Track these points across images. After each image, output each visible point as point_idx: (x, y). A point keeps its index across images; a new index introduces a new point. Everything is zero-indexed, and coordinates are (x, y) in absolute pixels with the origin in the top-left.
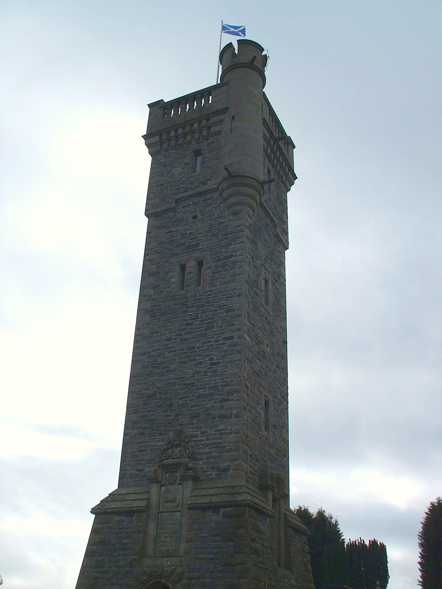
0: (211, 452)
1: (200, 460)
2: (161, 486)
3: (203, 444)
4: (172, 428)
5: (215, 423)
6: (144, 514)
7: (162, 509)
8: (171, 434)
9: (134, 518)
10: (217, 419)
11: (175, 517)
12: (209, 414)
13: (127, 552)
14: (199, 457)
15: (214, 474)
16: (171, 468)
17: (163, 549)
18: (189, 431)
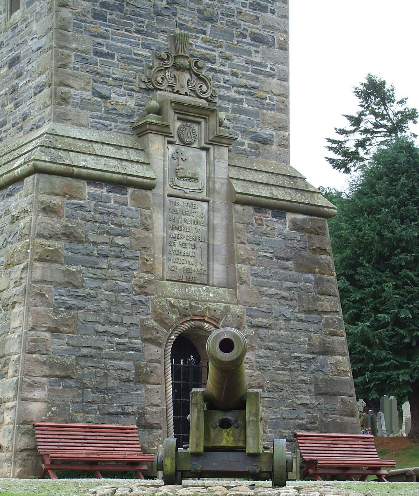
0: (241, 101)
1: (222, 109)
3: (226, 81)
4: (163, 27)
5: (246, 47)
8: (162, 40)
9: (128, 196)
10: (248, 40)
11: (199, 210)
12: (234, 24)
13: (126, 264)
15: (247, 142)
17: (180, 266)
18: (198, 45)
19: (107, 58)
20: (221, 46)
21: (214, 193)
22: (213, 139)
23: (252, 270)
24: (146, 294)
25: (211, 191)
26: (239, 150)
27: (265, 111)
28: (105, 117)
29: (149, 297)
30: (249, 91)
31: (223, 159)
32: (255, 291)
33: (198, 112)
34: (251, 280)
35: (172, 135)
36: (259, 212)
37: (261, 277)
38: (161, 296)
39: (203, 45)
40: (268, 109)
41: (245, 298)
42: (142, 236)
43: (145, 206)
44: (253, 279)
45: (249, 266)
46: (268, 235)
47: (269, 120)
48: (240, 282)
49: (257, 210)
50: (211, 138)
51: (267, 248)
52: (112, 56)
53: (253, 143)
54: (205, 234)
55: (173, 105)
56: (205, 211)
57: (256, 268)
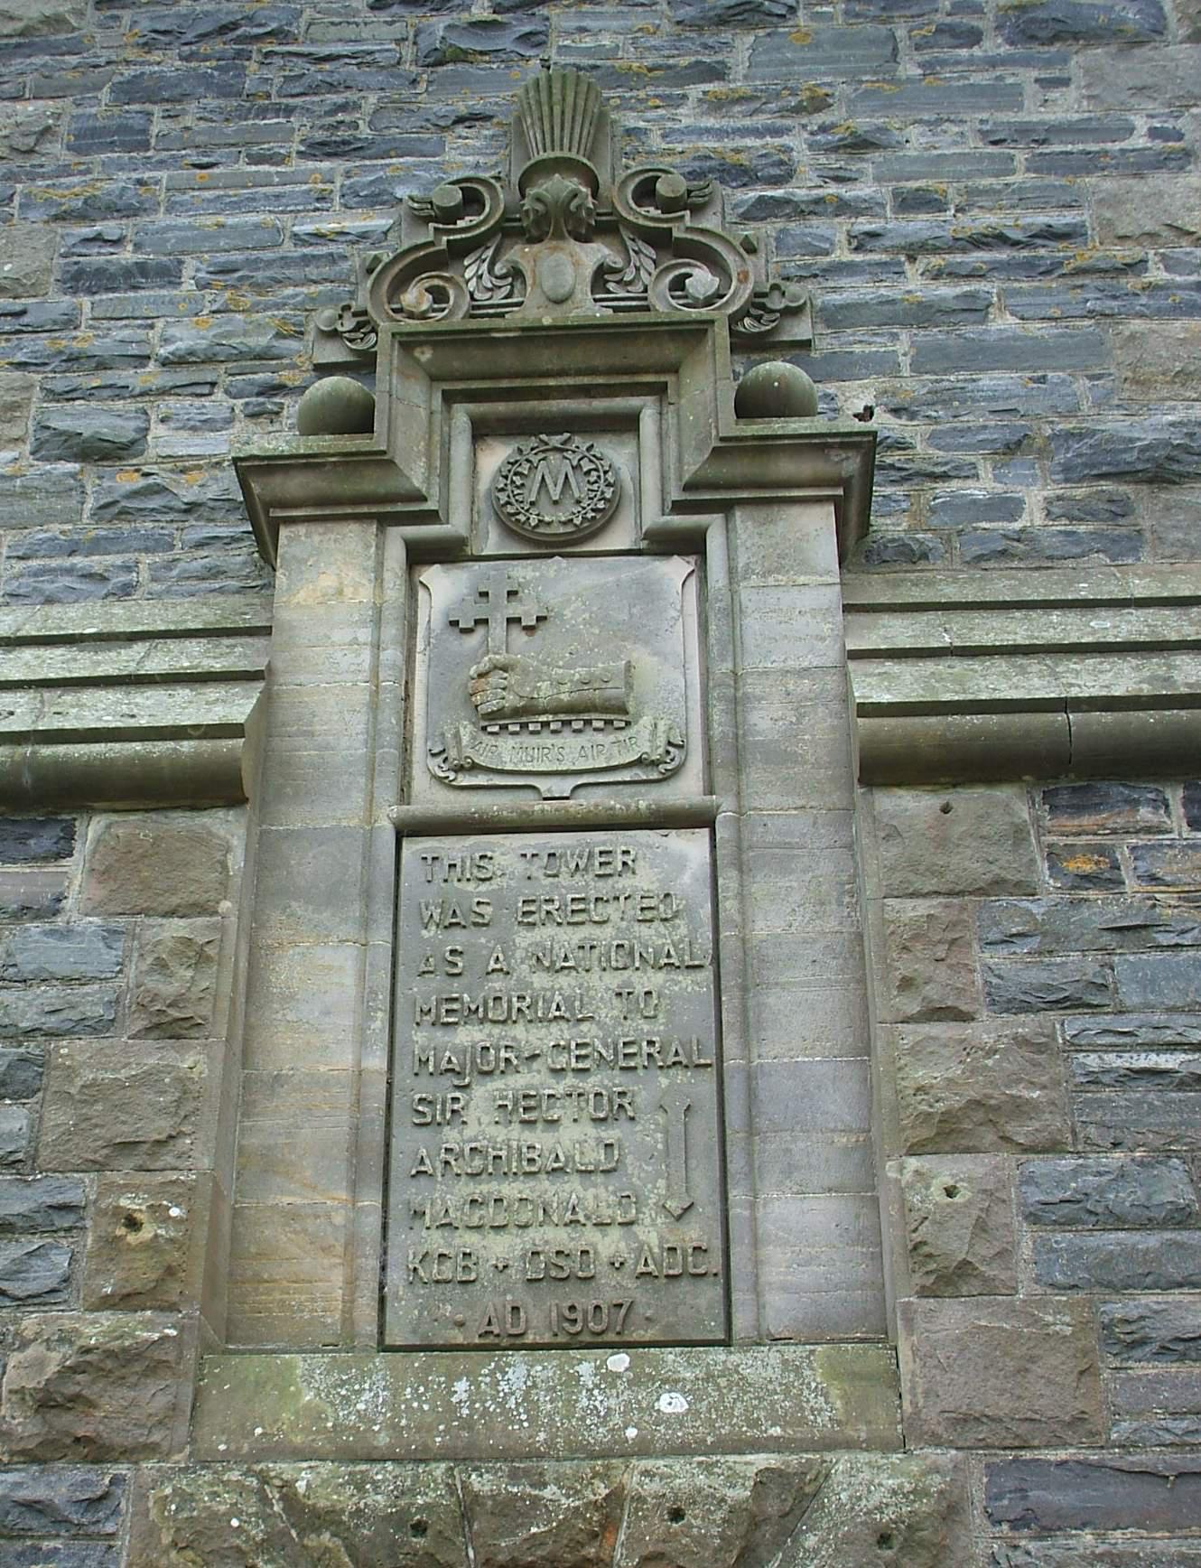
0: (975, 309)
2: (419, 555)
6: (226, 826)
7: (431, 799)
9: (75, 868)
10: (994, 45)
14: (826, 344)
16: (533, 387)
17: (499, 1247)
19: (135, 288)
20: (819, 103)
21: (738, 765)
22: (712, 472)
23: (1029, 1180)
24: (96, 1451)
25: (731, 755)
26: (981, 541)
27: (1137, 325)
28: (97, 540)
29: (122, 1469)
30: (1025, 253)
31: (805, 566)
32: (1062, 1325)
33: (598, 362)
34: (1026, 1250)
35: (431, 505)
36: (1079, 809)
37: (1117, 1221)
38: (225, 1458)
39: (710, 122)
40: (1160, 313)
41: (959, 1393)
42: (123, 1074)
43: (175, 900)
44: (1041, 1247)
45: (1006, 1159)
46: (1164, 939)
47: (1177, 358)
48: (918, 1279)
49: (1064, 798)
50: (690, 470)
51: (1159, 1018)
52: (168, 275)
53: (1080, 492)
54: (698, 1023)
55: (425, 355)
56: (686, 878)
57: (1068, 1163)
